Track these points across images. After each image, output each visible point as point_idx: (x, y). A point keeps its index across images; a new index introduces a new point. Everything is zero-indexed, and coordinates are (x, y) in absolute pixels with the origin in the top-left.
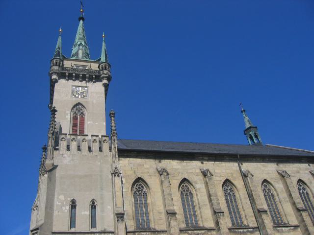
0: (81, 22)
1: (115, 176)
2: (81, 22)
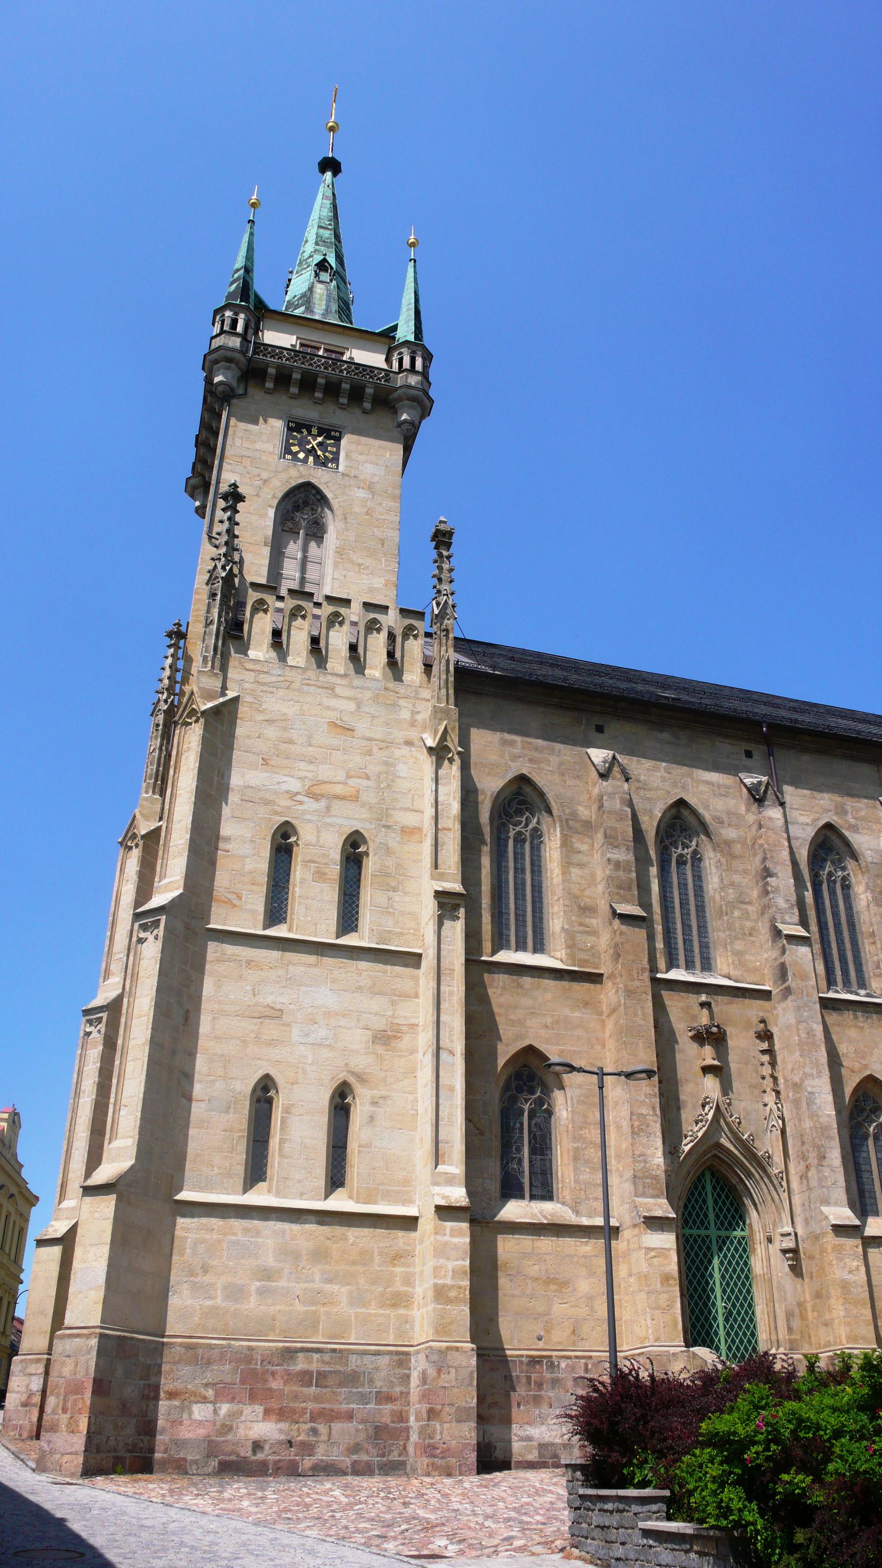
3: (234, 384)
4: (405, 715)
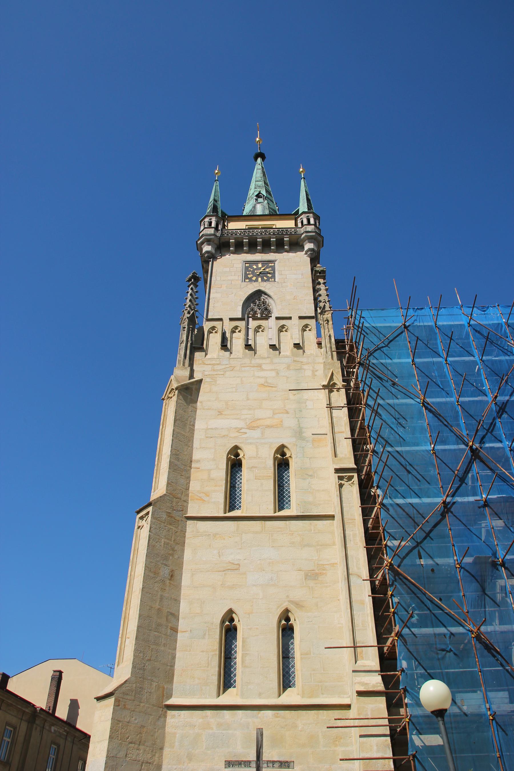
0: (259, 160)
1: (331, 391)
2: (259, 160)
3: (214, 251)
4: (309, 373)
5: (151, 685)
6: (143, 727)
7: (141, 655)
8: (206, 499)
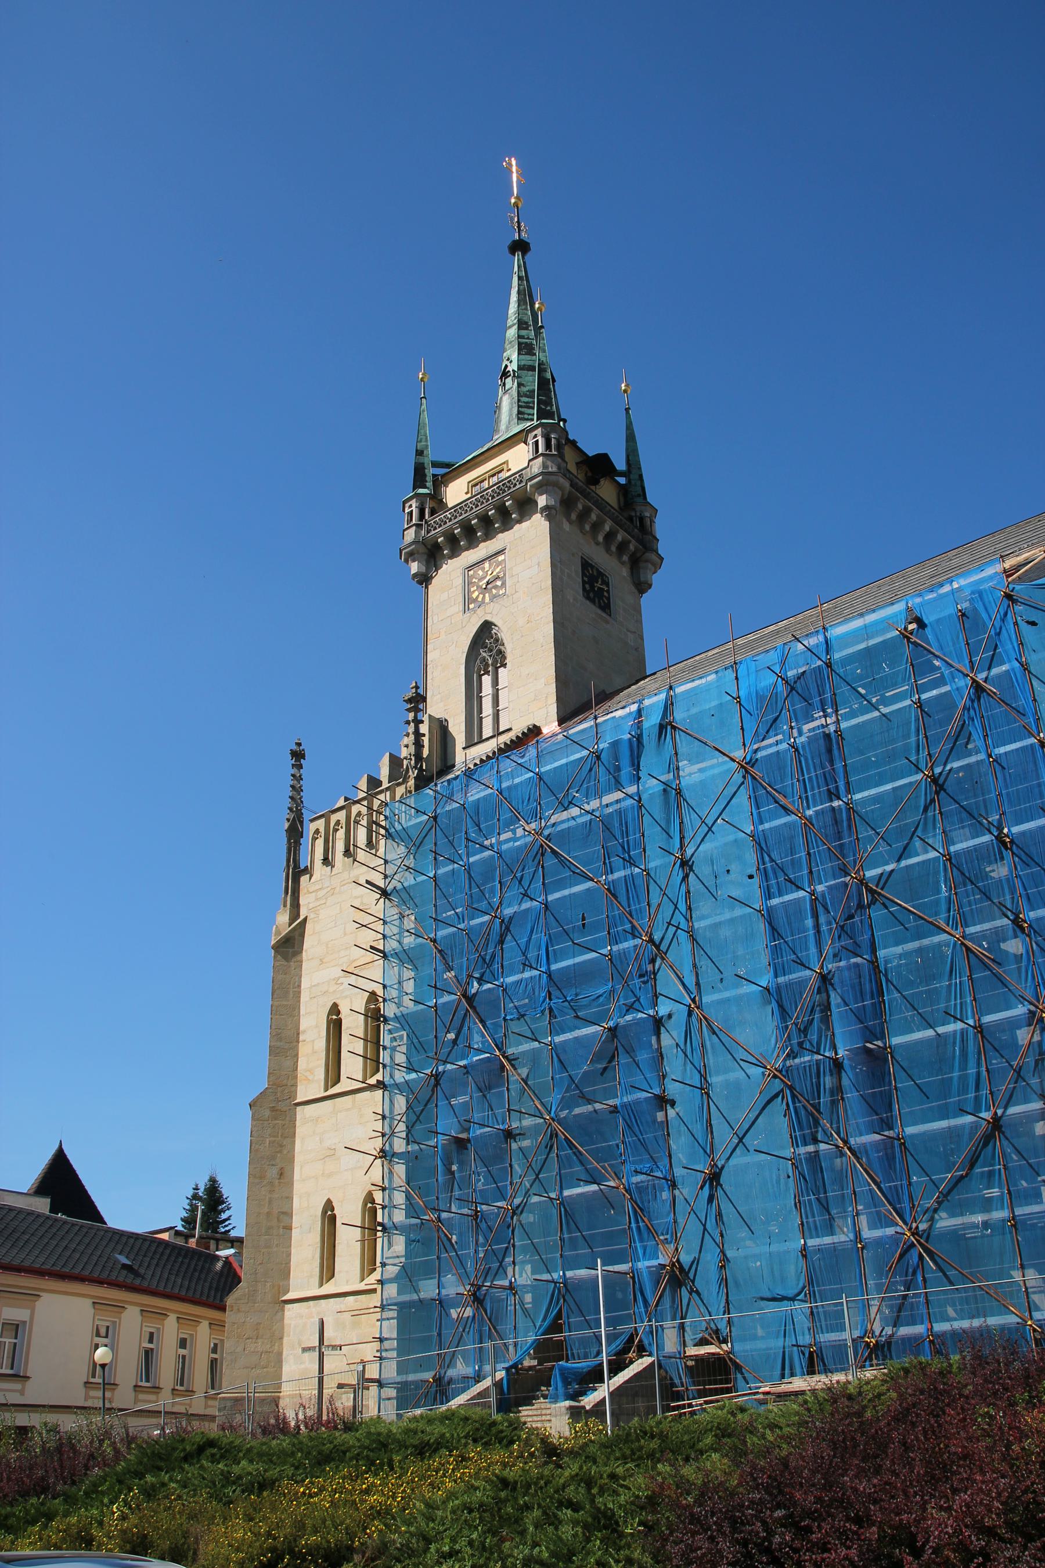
5: (265, 1285)
6: (259, 1324)
7: (252, 1261)
8: (311, 1077)
